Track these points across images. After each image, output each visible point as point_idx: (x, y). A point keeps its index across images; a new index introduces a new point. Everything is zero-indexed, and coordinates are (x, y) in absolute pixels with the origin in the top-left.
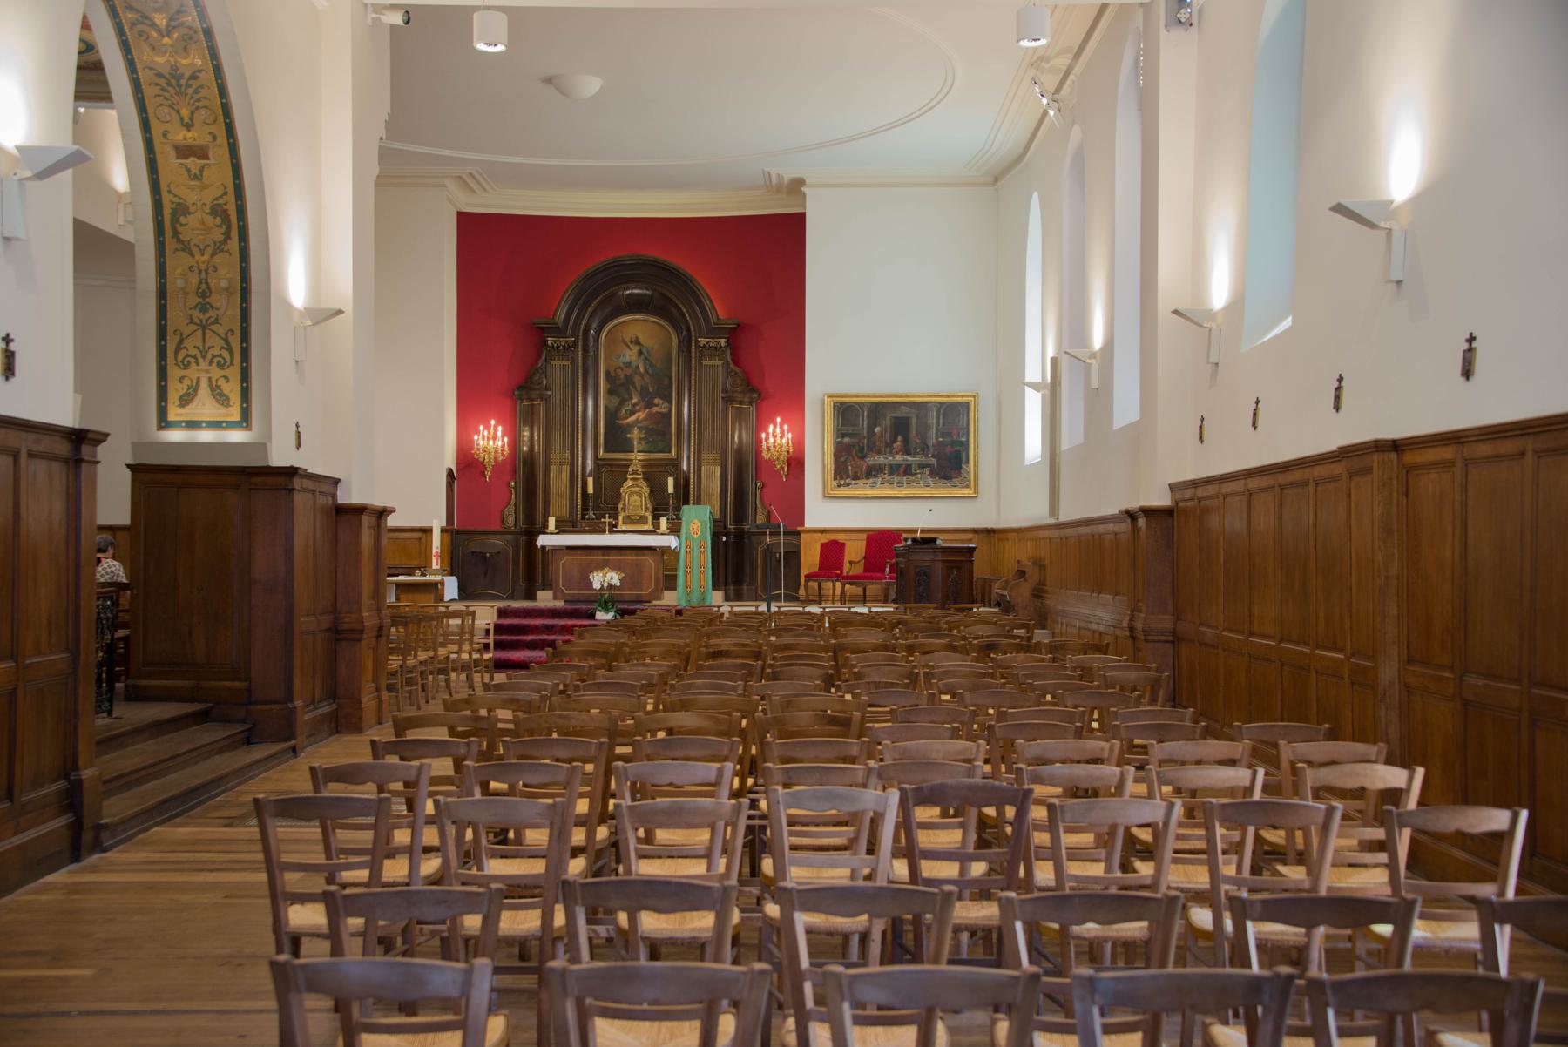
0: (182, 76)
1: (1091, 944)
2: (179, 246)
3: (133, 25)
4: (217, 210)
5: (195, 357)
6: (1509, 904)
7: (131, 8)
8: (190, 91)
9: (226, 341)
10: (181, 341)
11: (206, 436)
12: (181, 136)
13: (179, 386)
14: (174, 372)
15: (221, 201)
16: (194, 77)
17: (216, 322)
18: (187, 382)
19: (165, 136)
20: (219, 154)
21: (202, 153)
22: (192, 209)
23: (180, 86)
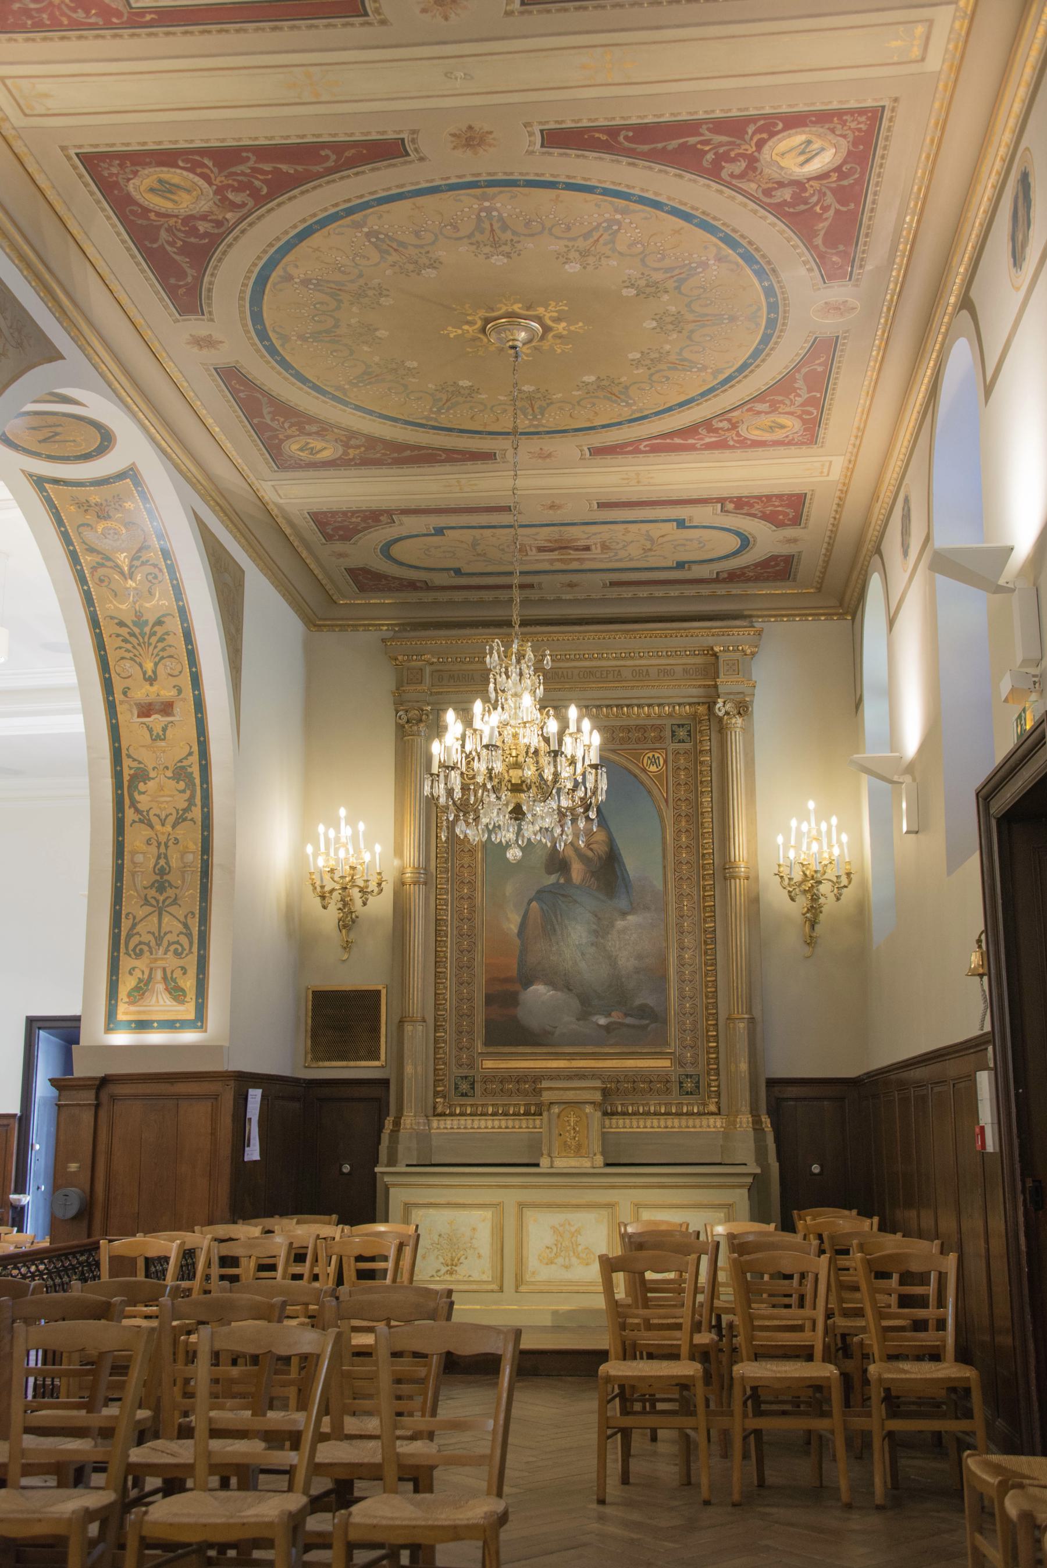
0: (146, 622)
1: (754, 1389)
2: (136, 817)
3: (94, 569)
4: (180, 773)
5: (148, 944)
6: (39, 1369)
7: (91, 550)
8: (154, 640)
9: (186, 925)
10: (134, 926)
11: (156, 1038)
12: (143, 693)
13: (130, 978)
14: (126, 962)
15: (185, 763)
16: (159, 622)
17: (175, 902)
18: (138, 974)
19: (125, 693)
20: (184, 711)
21: (167, 709)
22: (152, 774)
23: (143, 634)
